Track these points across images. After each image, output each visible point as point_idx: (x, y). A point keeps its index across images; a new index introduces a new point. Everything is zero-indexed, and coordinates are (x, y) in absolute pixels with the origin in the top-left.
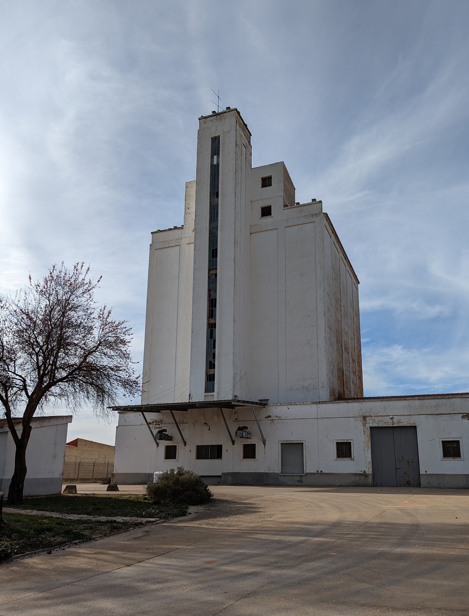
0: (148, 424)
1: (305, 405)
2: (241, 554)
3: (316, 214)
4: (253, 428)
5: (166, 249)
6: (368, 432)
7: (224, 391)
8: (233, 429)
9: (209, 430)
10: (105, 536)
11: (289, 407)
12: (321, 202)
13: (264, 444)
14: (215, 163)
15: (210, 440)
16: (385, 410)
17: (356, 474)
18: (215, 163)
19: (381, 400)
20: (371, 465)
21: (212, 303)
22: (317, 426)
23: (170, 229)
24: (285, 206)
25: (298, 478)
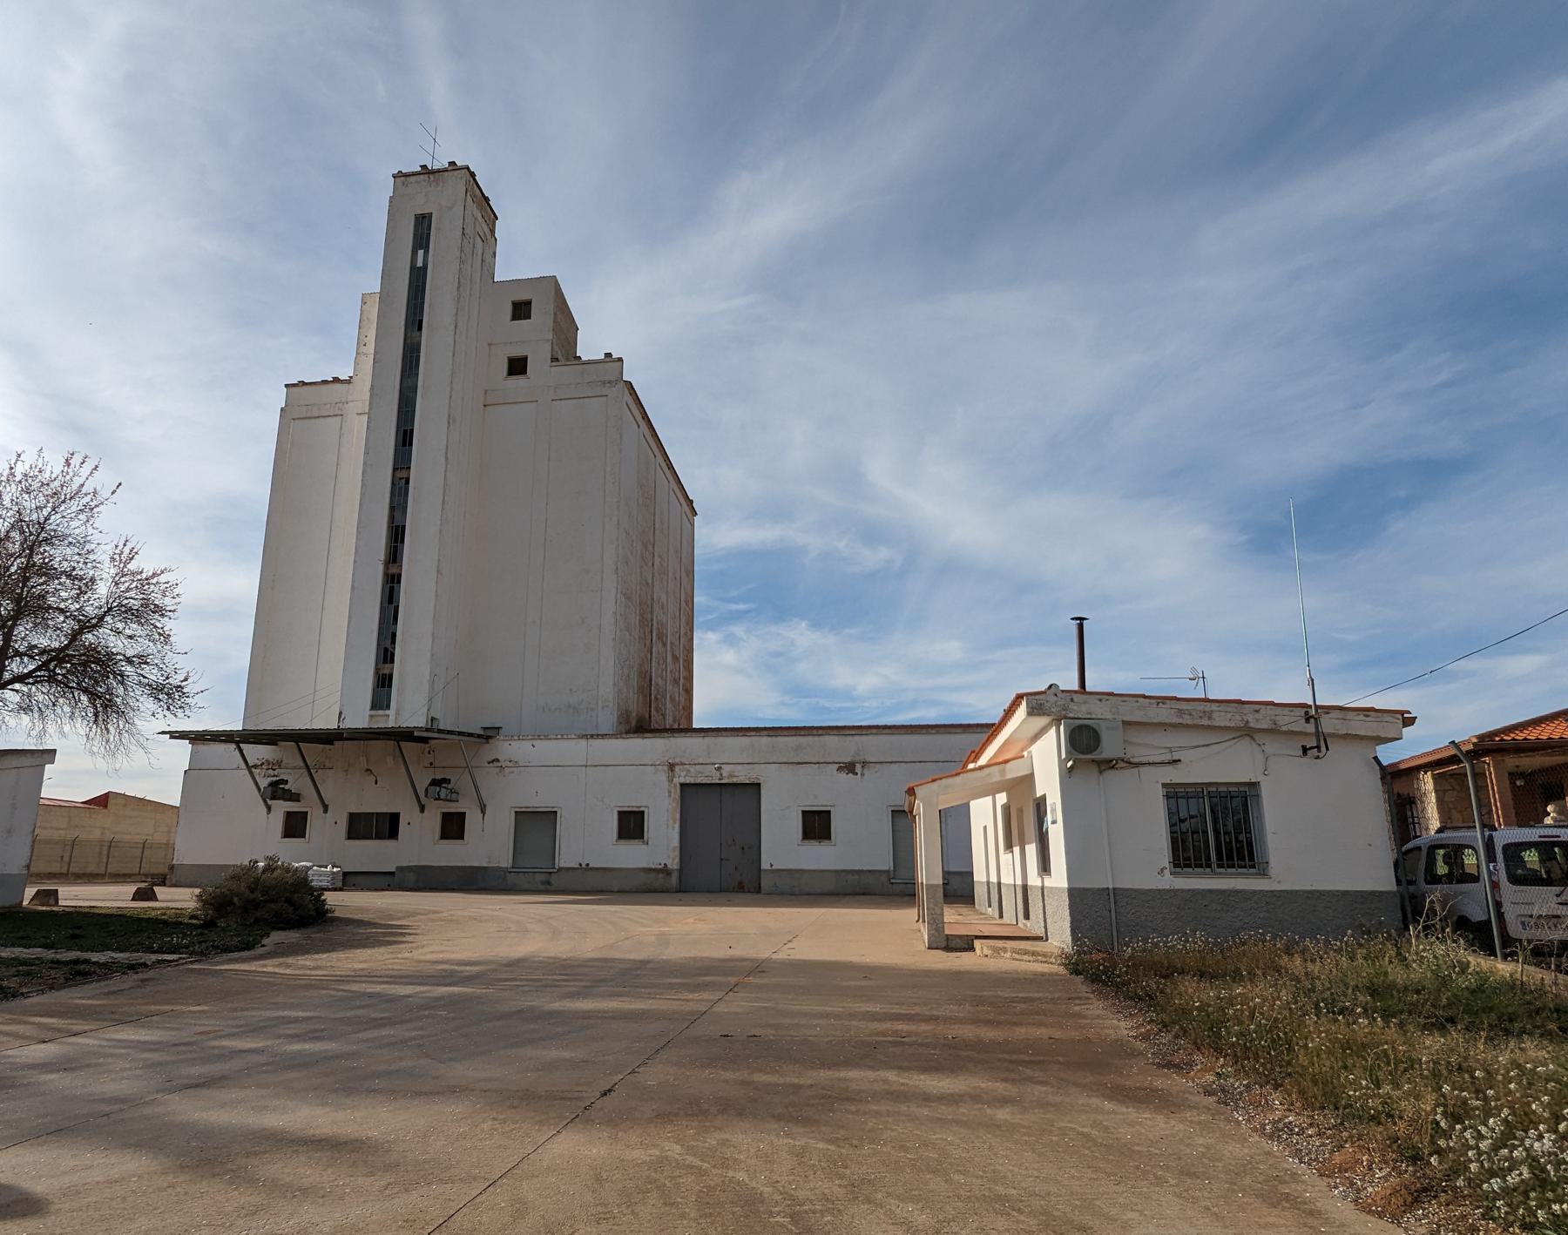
0: (249, 767)
2: (269, 1019)
4: (461, 781)
7: (408, 710)
8: (422, 783)
10: (52, 988)
12: (620, 360)
13: (483, 812)
14: (420, 264)
15: (375, 802)
17: (651, 870)
20: (677, 853)
21: (397, 534)
22: (588, 780)
24: (554, 359)
25: (543, 877)
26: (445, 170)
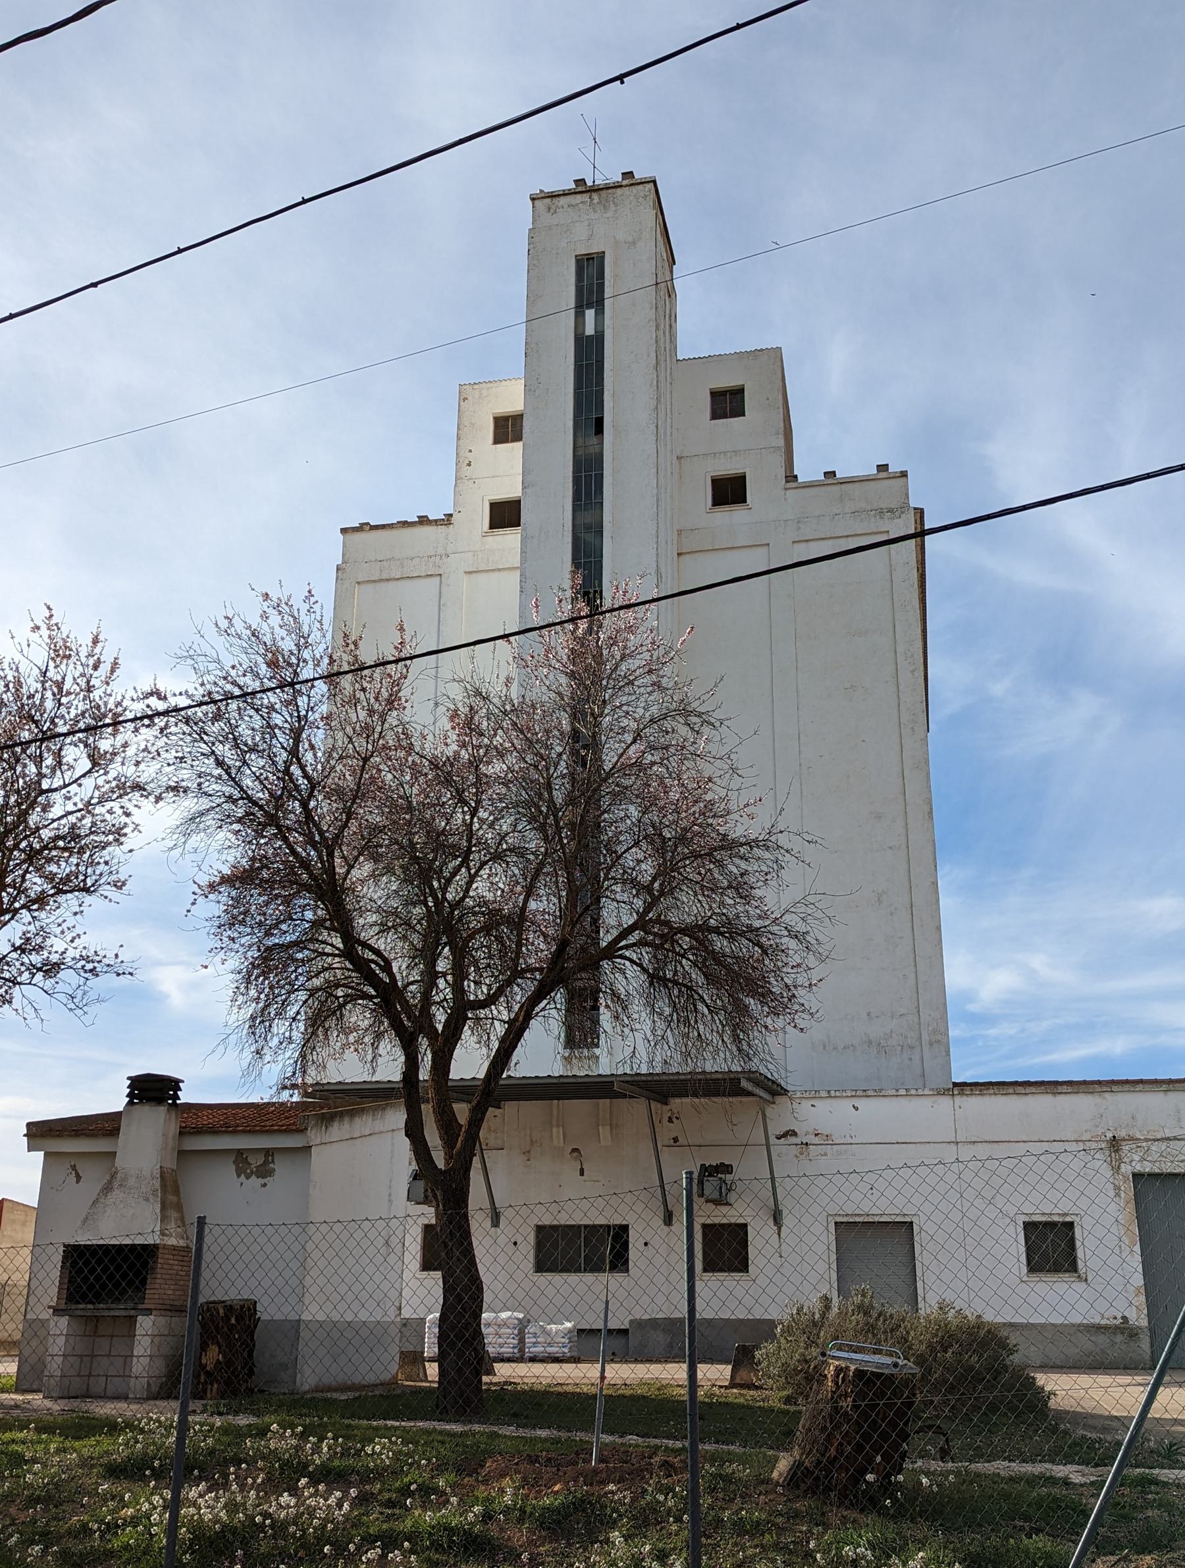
1: (914, 1101)
3: (891, 511)
4: (748, 1168)
5: (391, 585)
6: (1128, 1189)
9: (582, 1174)
11: (858, 1103)
12: (904, 474)
14: (590, 330)
15: (583, 1205)
16: (1179, 1120)
17: (1099, 1328)
18: (590, 330)
19: (1164, 1087)
23: (405, 524)
26: (618, 186)
